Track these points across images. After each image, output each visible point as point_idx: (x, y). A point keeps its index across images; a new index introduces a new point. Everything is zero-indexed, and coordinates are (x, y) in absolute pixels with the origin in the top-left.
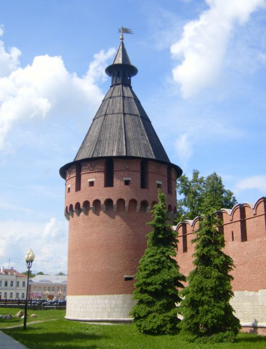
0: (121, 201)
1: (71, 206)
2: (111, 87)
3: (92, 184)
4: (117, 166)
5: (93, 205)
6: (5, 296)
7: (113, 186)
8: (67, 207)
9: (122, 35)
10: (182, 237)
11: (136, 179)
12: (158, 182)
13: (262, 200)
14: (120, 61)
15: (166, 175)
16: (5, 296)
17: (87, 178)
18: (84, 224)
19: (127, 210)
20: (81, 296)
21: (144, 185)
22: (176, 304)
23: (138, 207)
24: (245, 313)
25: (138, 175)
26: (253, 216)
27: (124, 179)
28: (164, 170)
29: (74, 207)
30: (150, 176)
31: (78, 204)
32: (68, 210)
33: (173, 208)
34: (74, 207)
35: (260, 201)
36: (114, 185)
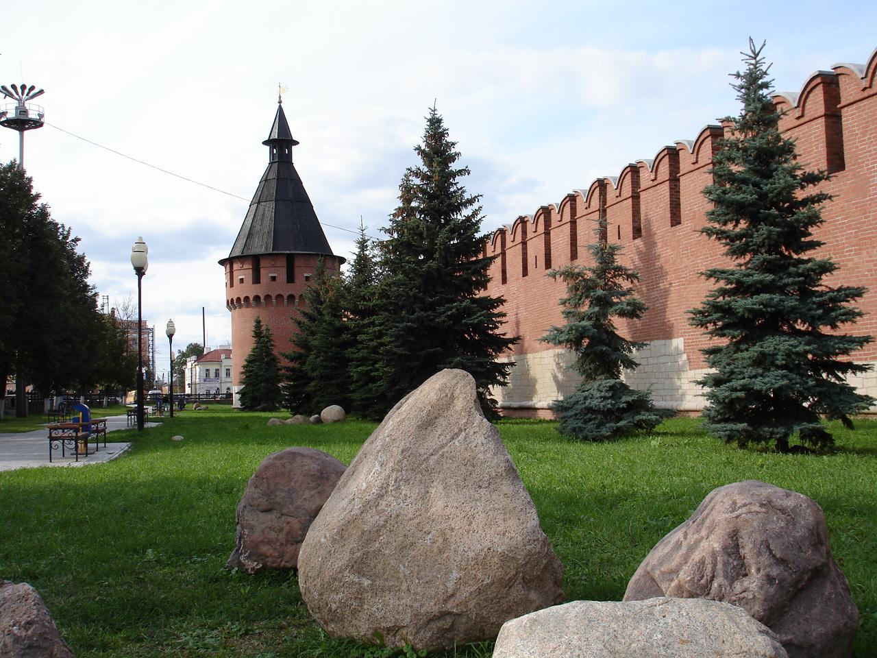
0: (247, 298)
3: (242, 281)
4: (263, 263)
5: (264, 300)
7: (260, 283)
10: (822, 120)
11: (282, 274)
12: (306, 275)
19: (275, 304)
21: (291, 278)
22: (625, 407)
25: (284, 270)
26: (652, 184)
27: (271, 275)
31: (238, 299)
34: (235, 302)
35: (566, 201)
36: (529, 274)
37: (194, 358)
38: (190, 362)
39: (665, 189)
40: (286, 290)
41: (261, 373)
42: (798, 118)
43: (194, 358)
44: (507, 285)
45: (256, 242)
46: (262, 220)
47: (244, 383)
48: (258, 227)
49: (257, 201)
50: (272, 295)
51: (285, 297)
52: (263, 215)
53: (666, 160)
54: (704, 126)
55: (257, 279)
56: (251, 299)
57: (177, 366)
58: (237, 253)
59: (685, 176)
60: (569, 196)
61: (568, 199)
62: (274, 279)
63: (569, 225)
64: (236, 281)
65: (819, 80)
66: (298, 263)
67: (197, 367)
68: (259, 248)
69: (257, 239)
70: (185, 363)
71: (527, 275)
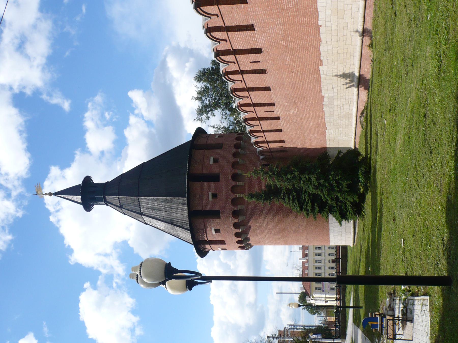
0: (236, 226)
1: (238, 242)
2: (107, 205)
3: (217, 231)
4: (198, 207)
5: (239, 229)
6: (332, 255)
8: (240, 247)
9: (46, 194)
11: (210, 188)
12: (211, 162)
13: (198, 9)
14: (78, 198)
15: (203, 151)
16: (332, 255)
17: (212, 235)
18: (259, 235)
19: (243, 207)
20: (330, 236)
21: (215, 178)
23: (239, 183)
24: (344, 103)
27: (210, 199)
28: (199, 154)
29: (240, 239)
30: (206, 171)
31: (237, 235)
32: (242, 245)
33: (238, 136)
34: (240, 239)
35: (201, 12)
36: (217, 209)
37: (307, 298)
38: (311, 301)
39: (239, 57)
40: (227, 182)
41: (314, 180)
42: (218, 17)
43: (307, 298)
44: (275, 104)
45: (177, 215)
46: (157, 210)
47: (327, 217)
48: (164, 214)
49: (140, 216)
50: (231, 197)
51: (234, 183)
52: (152, 209)
53: (213, 34)
54: (194, 11)
55: (215, 214)
56: (236, 221)
57: (314, 309)
58: (188, 235)
59: (247, 84)
60: (206, 32)
61: (208, 34)
62: (214, 196)
63: (237, 56)
64: (218, 238)
65: (198, 9)
66: (198, 170)
67: (314, 296)
68: (182, 213)
69: (175, 215)
70: (311, 305)
71: (269, 87)
